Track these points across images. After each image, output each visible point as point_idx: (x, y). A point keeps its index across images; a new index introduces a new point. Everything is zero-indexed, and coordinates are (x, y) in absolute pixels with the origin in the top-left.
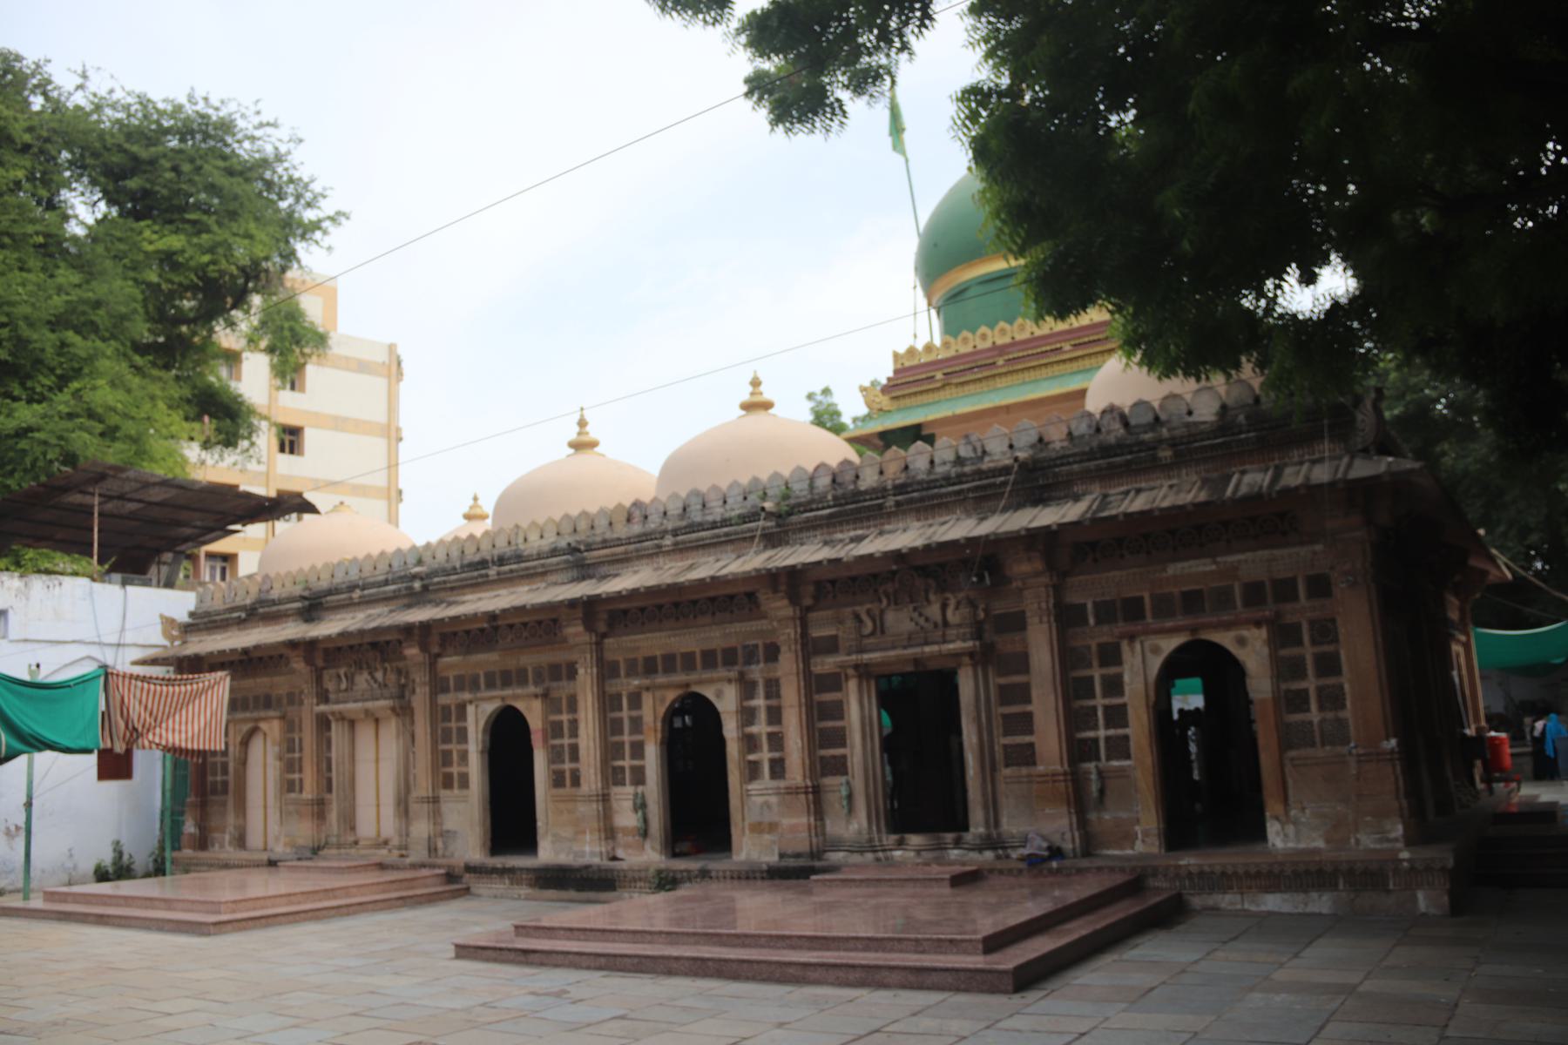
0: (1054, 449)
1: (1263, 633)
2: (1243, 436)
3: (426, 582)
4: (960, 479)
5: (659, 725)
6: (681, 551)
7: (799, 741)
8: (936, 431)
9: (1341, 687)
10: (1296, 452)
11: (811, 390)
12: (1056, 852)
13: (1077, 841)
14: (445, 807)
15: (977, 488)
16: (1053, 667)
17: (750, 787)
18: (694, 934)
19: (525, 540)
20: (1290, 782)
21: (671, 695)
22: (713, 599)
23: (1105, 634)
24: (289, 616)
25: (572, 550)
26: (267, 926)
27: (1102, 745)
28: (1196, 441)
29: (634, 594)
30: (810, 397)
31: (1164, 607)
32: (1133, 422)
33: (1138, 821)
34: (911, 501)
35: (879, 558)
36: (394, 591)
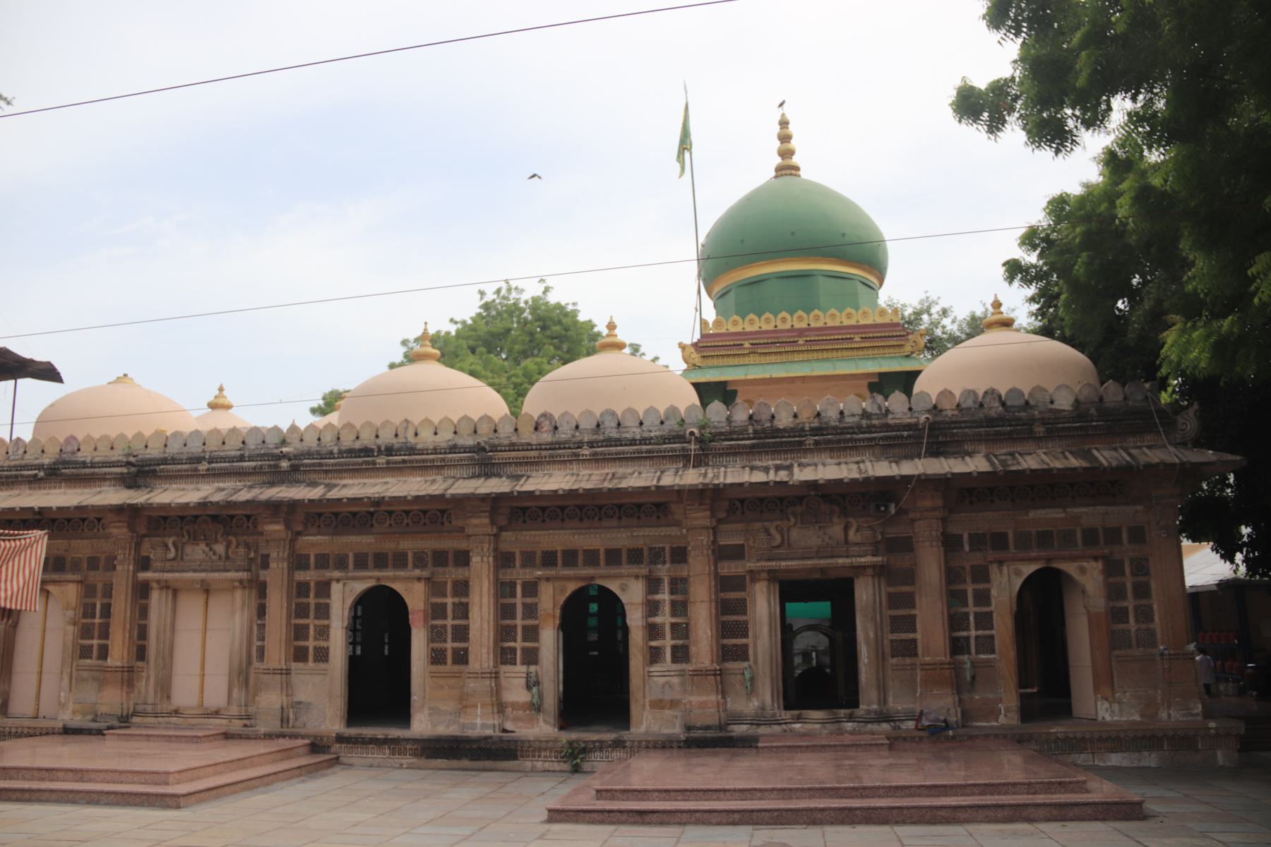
0: (946, 416)
1: (1100, 565)
2: (1094, 423)
3: (296, 462)
4: (870, 429)
5: (558, 612)
6: (597, 461)
7: (709, 631)
8: (739, 389)
9: (1151, 607)
10: (1131, 439)
11: (406, 337)
12: (947, 726)
13: (959, 715)
14: (296, 679)
15: (887, 438)
16: (941, 581)
17: (651, 669)
18: (810, 789)
19: (416, 434)
20: (1115, 672)
21: (572, 587)
22: (620, 506)
23: (977, 559)
24: (105, 480)
25: (479, 449)
26: (217, 797)
27: (973, 642)
28: (1059, 423)
29: (545, 496)
30: (404, 343)
31: (1024, 541)
32: (1009, 403)
33: (1000, 700)
34: (829, 442)
35: (847, 483)
36: (255, 468)
